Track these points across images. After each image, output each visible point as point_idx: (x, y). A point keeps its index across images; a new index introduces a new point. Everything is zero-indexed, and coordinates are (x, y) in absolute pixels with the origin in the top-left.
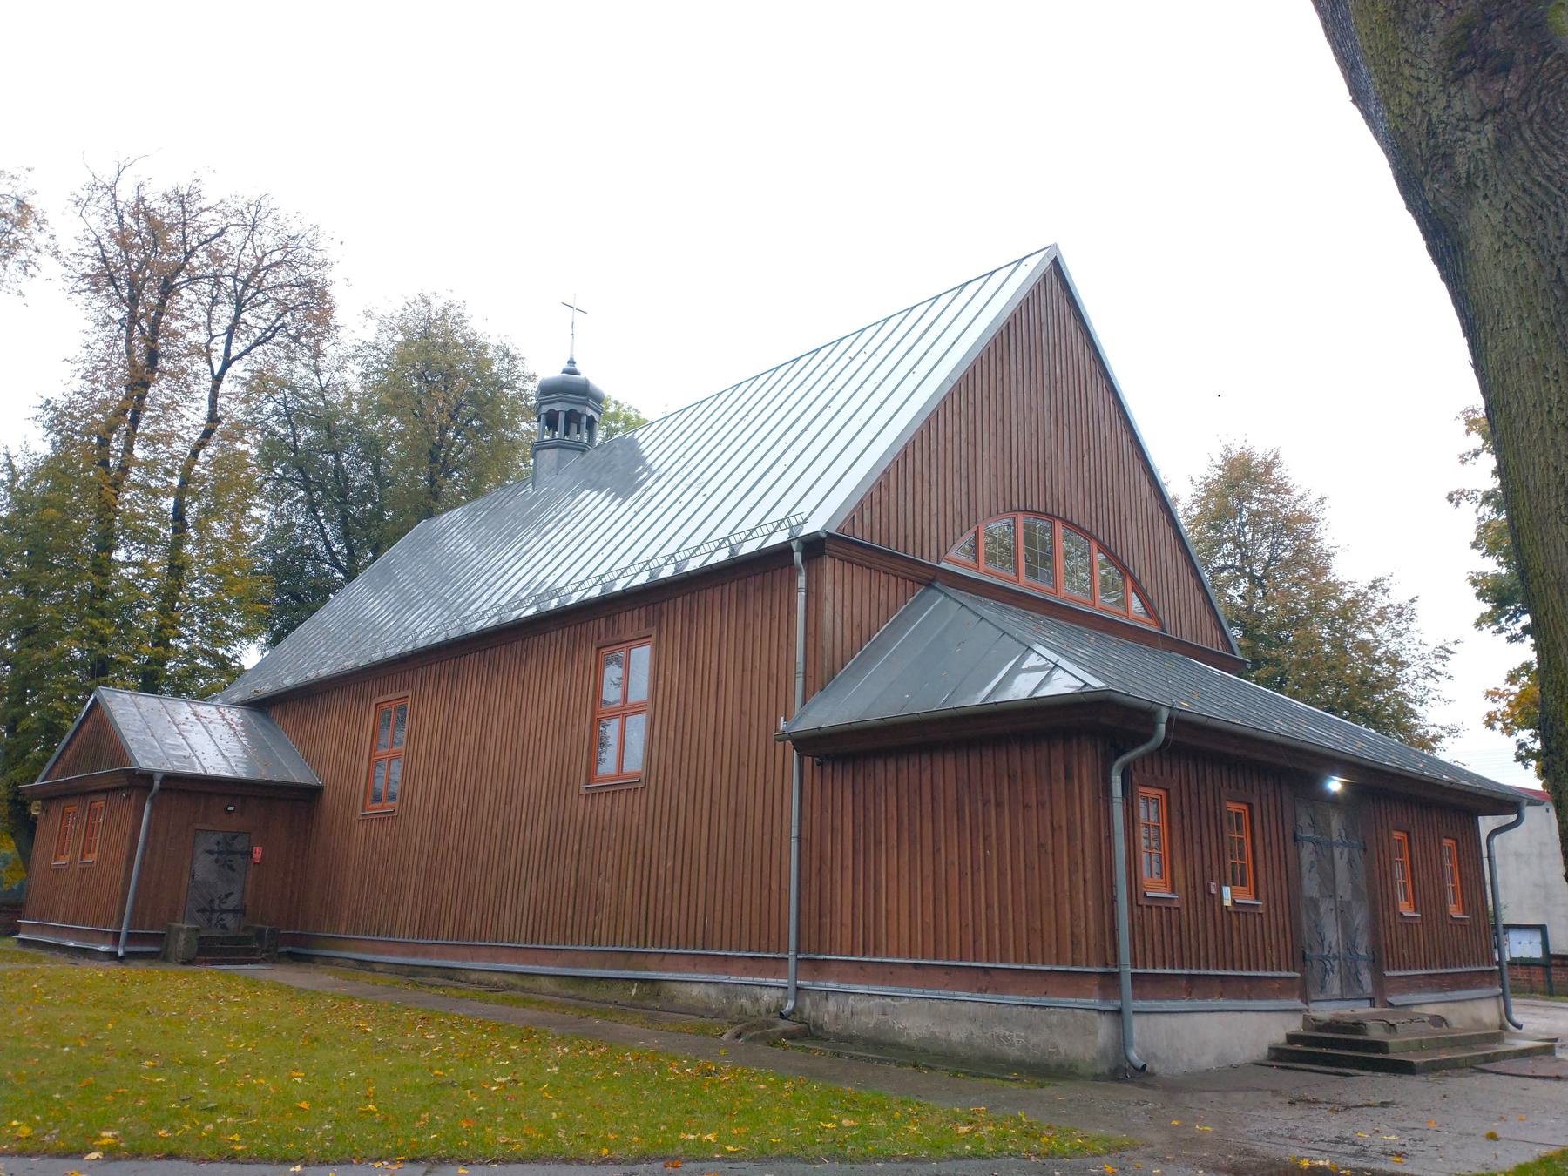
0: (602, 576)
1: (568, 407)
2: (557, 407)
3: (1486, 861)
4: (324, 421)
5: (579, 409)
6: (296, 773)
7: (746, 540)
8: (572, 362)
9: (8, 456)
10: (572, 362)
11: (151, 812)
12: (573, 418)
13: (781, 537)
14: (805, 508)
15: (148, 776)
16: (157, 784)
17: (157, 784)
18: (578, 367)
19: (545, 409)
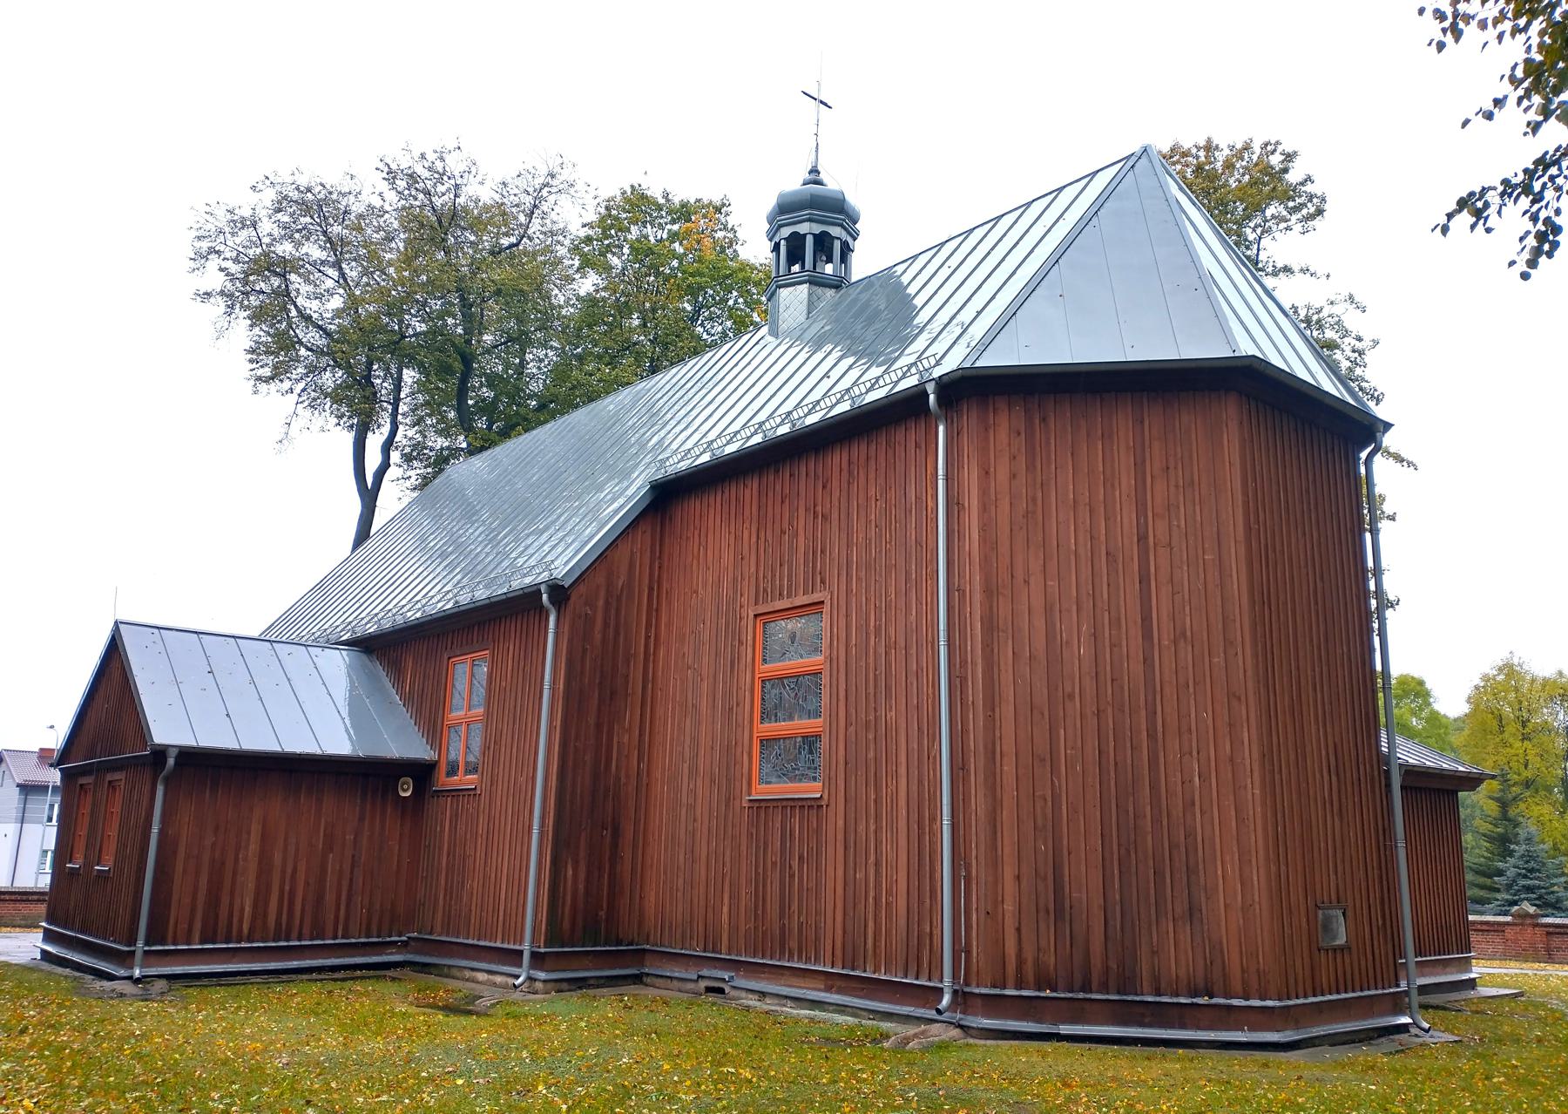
0: (761, 424)
1: (817, 229)
2: (803, 228)
3: (1376, 640)
4: (643, 197)
5: (835, 231)
6: (400, 741)
7: (877, 379)
8: (814, 170)
9: (1532, 263)
10: (814, 170)
11: (165, 795)
12: (823, 244)
13: (912, 381)
14: (939, 348)
15: (160, 753)
16: (171, 762)
17: (171, 762)
18: (823, 176)
19: (786, 232)
